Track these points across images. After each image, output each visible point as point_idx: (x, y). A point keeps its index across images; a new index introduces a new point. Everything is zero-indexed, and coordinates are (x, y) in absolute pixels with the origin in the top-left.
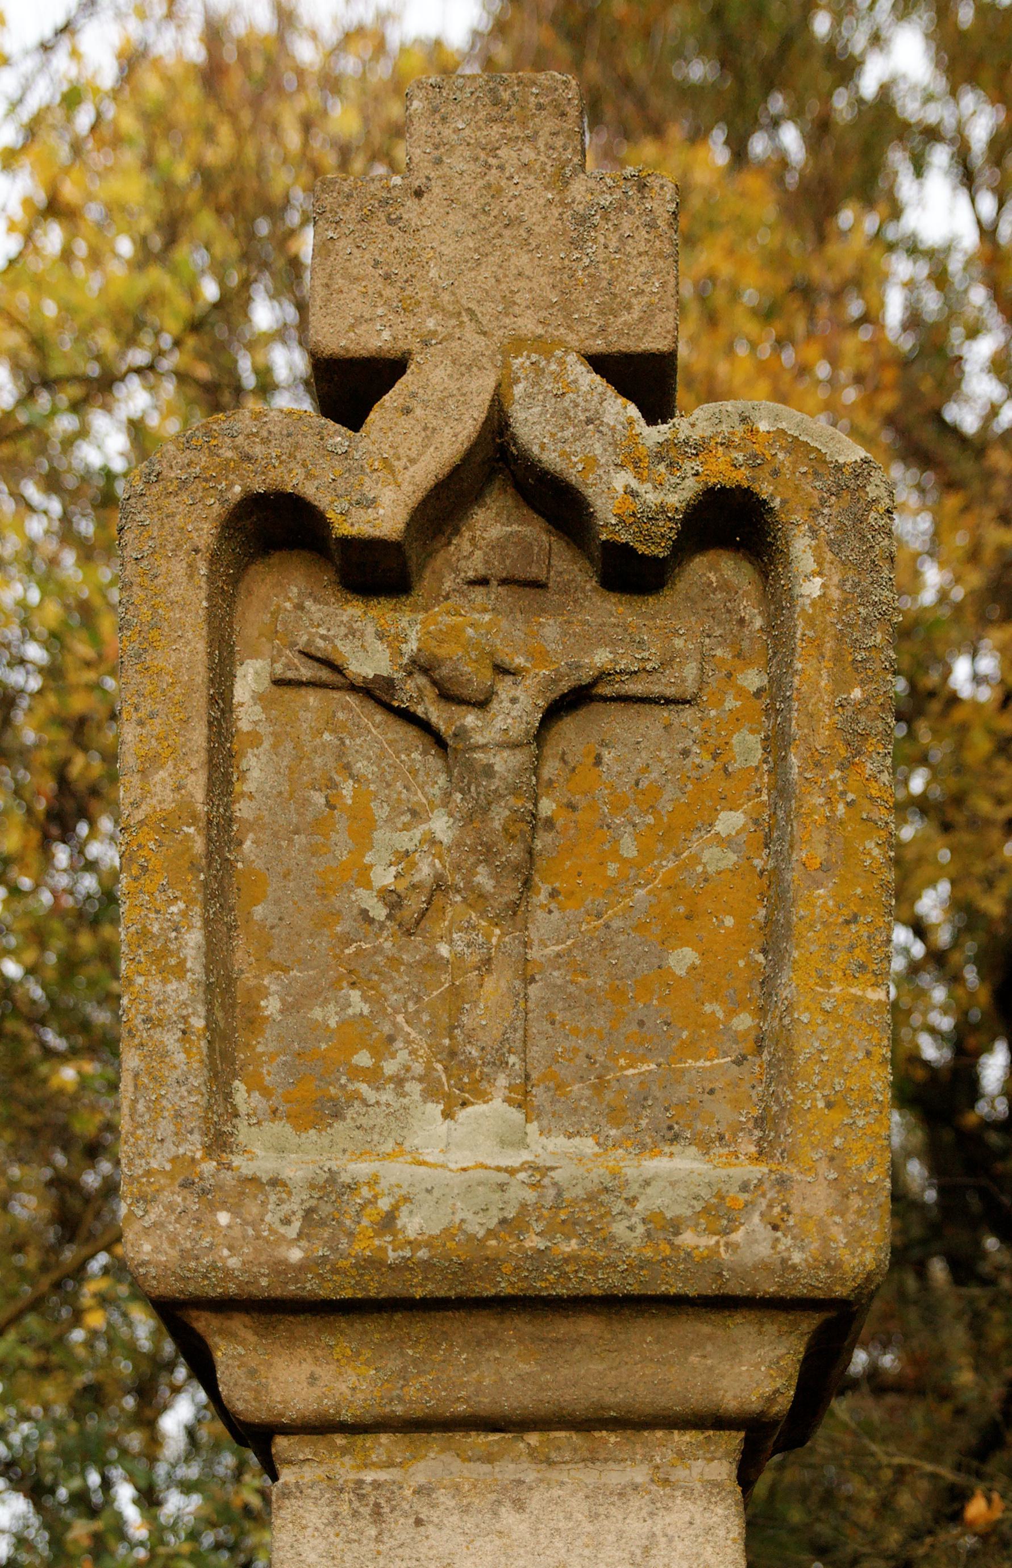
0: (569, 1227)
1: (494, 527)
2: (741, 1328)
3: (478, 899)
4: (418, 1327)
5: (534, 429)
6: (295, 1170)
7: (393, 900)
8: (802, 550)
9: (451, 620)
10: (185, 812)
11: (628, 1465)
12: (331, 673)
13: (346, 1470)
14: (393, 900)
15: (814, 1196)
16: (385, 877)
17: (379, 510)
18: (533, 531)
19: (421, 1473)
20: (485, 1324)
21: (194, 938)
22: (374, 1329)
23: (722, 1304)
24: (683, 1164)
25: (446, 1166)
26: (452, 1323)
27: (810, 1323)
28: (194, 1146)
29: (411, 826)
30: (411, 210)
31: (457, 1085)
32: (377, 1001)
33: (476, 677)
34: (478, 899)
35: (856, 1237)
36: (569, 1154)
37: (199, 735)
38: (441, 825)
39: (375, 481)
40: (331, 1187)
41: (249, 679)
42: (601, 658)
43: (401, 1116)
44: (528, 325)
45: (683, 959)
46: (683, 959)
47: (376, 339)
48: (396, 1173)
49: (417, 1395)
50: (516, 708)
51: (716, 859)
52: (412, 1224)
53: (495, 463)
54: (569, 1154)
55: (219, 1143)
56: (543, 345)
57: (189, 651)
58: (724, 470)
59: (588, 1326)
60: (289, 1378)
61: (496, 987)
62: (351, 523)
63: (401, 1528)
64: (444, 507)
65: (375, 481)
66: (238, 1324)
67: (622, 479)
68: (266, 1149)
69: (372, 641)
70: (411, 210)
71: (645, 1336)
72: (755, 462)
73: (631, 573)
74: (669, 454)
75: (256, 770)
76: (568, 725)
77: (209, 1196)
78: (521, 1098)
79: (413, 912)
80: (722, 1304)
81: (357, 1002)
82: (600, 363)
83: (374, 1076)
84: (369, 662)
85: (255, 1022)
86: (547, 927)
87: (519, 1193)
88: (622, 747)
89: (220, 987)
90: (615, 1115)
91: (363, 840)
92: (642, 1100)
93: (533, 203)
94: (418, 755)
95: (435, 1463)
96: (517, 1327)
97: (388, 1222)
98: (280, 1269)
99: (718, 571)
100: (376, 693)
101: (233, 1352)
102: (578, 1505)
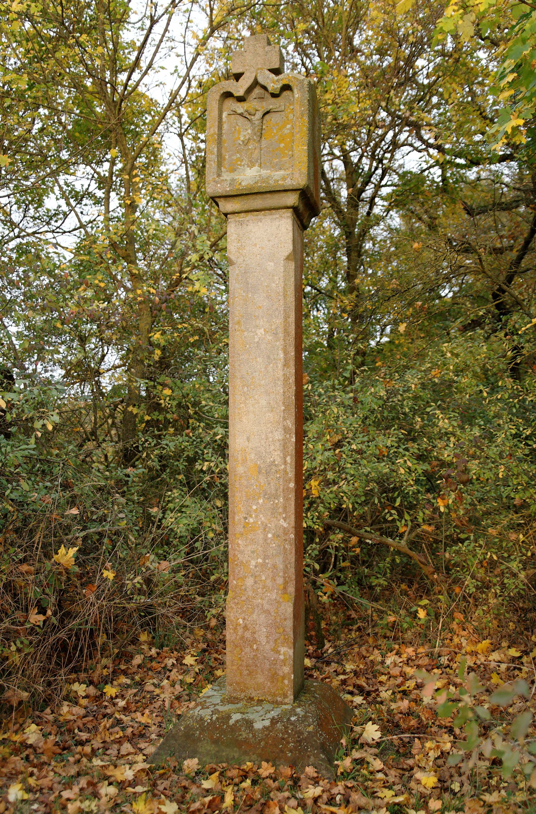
0: (264, 182)
1: (257, 91)
2: (289, 194)
3: (254, 140)
4: (246, 197)
5: (261, 80)
6: (228, 178)
7: (243, 142)
8: (295, 91)
9: (252, 104)
10: (215, 133)
11: (276, 214)
12: (235, 113)
13: (237, 219)
14: (243, 142)
15: (297, 175)
16: (242, 139)
17: (240, 92)
18: (262, 91)
19: (247, 218)
20: (254, 196)
21: (216, 149)
22: (240, 198)
23: (286, 191)
24: (282, 172)
25: (249, 176)
26: (250, 196)
27: (299, 192)
28: (215, 176)
29: (246, 131)
30: (245, 54)
31: (251, 165)
32: (241, 155)
33: (253, 112)
34: (254, 140)
35: (302, 180)
36: (265, 172)
37: (217, 123)
38: (249, 131)
39: (239, 88)
40: (233, 180)
41: (225, 115)
42: (271, 107)
43: (244, 170)
44: (260, 66)
45: (282, 145)
46: (282, 145)
47: (240, 71)
48: (241, 177)
49: (246, 207)
50: (259, 115)
51: (286, 132)
52: (243, 184)
53: (256, 83)
54: (265, 172)
55: (219, 176)
56: (261, 69)
57: (216, 113)
58: (285, 82)
59: (268, 195)
60: (227, 206)
61: (257, 151)
62: (236, 94)
63: (245, 226)
64: (250, 90)
65: (239, 88)
66: (222, 199)
67: (272, 85)
68: (226, 176)
69: (240, 108)
70: (245, 54)
71: (277, 196)
72: (289, 80)
73: (274, 96)
74: (278, 81)
75: (225, 126)
76: (267, 116)
77: (217, 183)
78: (260, 166)
79: (246, 143)
80: (286, 191)
81: (238, 155)
82: (270, 70)
83: (240, 165)
84: (239, 112)
85: (225, 159)
86: (264, 143)
87: (258, 178)
88: (272, 118)
89: (220, 155)
90: (273, 167)
91: (239, 134)
92: (277, 164)
93: (260, 51)
94: (247, 122)
95: (250, 216)
96: (259, 196)
97: (240, 184)
98: (226, 191)
99: (286, 93)
100: (241, 115)
101: (221, 202)
102: (269, 221)
